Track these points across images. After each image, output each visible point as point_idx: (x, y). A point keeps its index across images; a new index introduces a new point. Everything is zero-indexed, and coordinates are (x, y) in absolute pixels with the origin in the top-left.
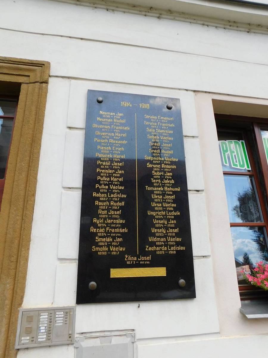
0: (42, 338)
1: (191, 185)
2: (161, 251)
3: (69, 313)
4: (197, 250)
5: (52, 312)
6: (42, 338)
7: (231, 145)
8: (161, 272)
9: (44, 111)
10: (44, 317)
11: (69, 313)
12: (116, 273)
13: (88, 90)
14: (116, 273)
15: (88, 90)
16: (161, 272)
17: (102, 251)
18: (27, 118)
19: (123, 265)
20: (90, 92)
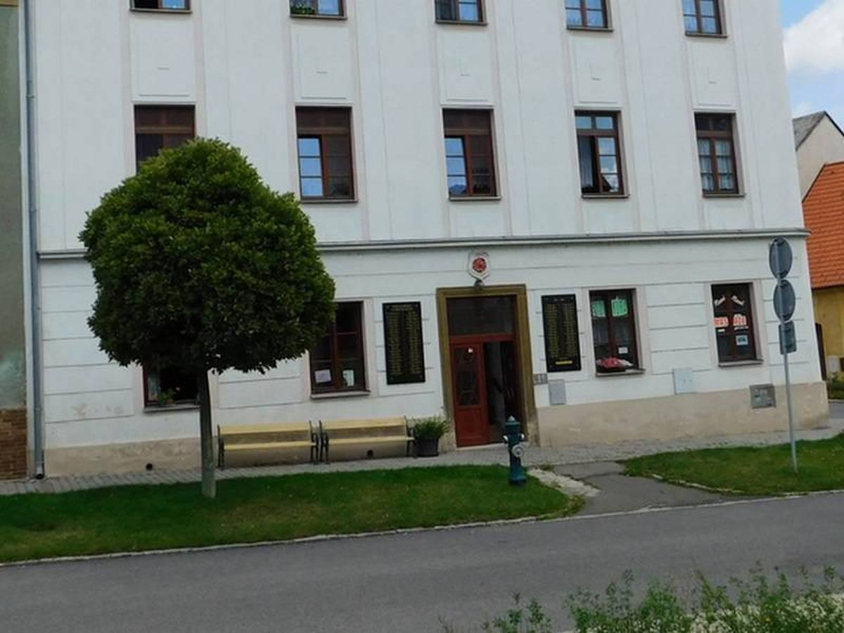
0: (540, 381)
1: (580, 331)
2: (570, 355)
3: (545, 375)
4: (582, 354)
5: (541, 375)
6: (540, 381)
7: (571, 404)
8: (570, 362)
9: (220, 143)
10: (539, 377)
11: (545, 375)
12: (558, 363)
13: (423, 380)
14: (558, 363)
15: (423, 380)
16: (570, 362)
17: (553, 357)
18: (234, 328)
19: (559, 361)
20: (416, 307)
